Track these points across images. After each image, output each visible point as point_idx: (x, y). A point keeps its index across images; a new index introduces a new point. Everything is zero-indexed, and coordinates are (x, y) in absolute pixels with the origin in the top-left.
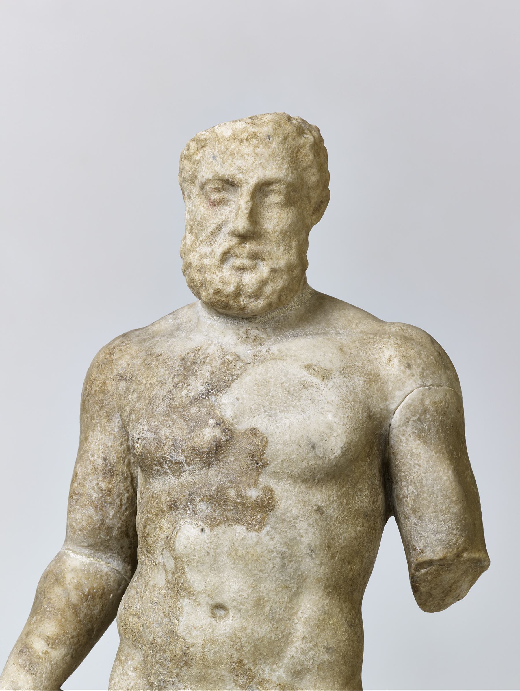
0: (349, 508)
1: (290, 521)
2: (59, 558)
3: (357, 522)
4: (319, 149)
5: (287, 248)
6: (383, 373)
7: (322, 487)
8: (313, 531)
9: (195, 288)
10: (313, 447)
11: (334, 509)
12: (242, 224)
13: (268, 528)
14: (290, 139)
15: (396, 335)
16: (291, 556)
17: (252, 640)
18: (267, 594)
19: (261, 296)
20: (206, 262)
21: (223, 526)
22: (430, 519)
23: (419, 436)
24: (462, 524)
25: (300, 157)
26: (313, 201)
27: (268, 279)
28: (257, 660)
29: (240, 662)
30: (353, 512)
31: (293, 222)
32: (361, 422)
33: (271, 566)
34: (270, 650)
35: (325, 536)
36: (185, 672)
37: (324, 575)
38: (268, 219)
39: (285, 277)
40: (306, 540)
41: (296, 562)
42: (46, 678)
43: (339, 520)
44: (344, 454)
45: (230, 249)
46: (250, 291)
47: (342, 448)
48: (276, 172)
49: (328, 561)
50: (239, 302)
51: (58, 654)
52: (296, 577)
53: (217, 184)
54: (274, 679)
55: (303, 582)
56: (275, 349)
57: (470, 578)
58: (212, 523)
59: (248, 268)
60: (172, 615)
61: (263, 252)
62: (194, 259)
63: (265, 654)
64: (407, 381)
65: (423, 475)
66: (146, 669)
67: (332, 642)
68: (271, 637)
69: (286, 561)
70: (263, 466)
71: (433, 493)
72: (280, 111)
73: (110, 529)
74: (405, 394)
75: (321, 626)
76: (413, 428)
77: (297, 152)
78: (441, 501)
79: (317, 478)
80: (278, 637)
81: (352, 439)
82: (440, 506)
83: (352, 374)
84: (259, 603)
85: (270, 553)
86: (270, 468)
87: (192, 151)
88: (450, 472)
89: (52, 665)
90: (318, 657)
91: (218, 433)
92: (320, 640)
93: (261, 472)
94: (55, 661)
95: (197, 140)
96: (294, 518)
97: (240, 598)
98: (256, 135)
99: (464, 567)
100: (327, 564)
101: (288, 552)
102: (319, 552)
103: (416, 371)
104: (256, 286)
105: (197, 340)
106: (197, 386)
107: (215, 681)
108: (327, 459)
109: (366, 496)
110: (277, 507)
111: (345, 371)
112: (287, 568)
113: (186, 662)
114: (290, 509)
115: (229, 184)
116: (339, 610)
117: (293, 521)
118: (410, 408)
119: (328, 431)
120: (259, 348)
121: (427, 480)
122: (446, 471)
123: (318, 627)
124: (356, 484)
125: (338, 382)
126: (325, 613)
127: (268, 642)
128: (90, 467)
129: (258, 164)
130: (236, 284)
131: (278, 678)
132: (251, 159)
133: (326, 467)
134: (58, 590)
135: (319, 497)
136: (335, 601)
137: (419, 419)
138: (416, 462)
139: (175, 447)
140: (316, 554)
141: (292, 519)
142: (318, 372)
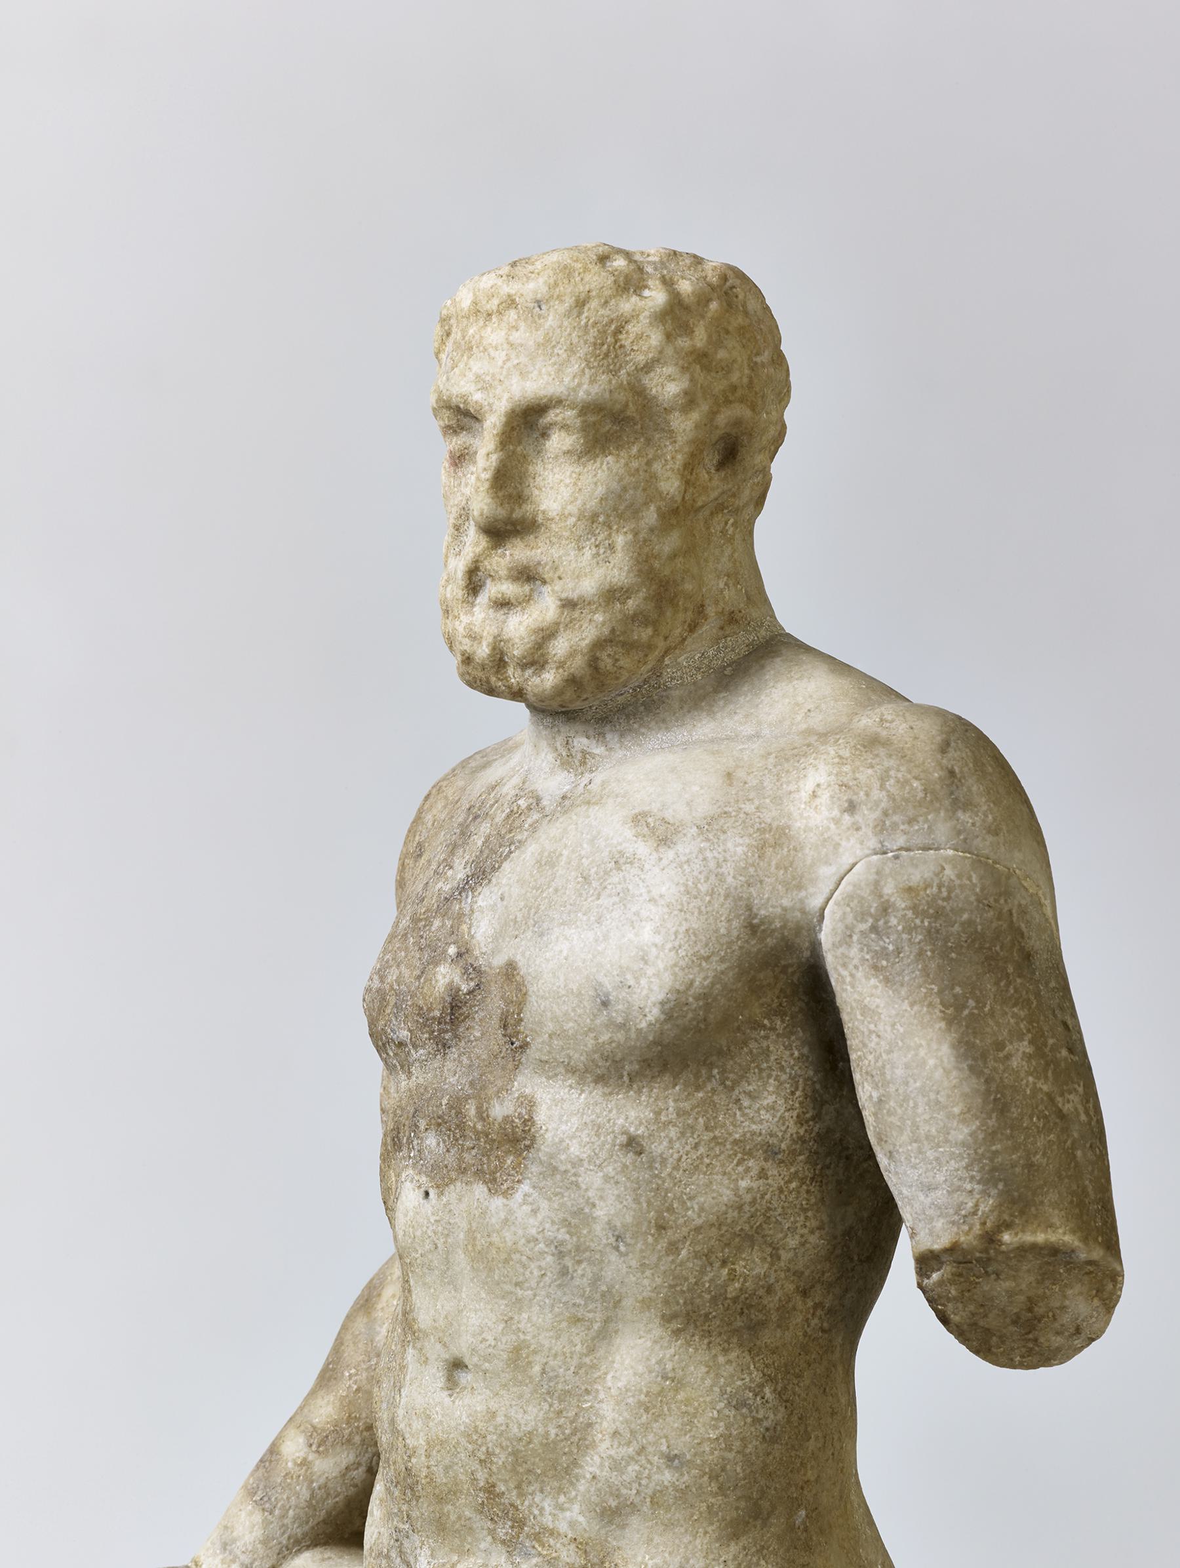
0: (715, 1138)
1: (566, 1172)
3: (740, 1169)
5: (602, 551)
6: (798, 824)
7: (639, 1092)
8: (616, 1192)
10: (605, 1004)
11: (671, 1141)
13: (525, 1187)
14: (594, 304)
17: (508, 1439)
18: (534, 1337)
19: (546, 662)
21: (458, 1184)
22: (908, 1159)
24: (983, 1168)
25: (627, 343)
26: (681, 439)
27: (558, 624)
28: (524, 1486)
29: (490, 1489)
30: (728, 1146)
31: (609, 491)
32: (725, 940)
33: (536, 1273)
35: (649, 1203)
38: (552, 488)
39: (599, 618)
41: (591, 1262)
42: (296, 1518)
43: (684, 1165)
45: (477, 561)
46: (515, 653)
47: (662, 1003)
48: (548, 383)
49: (659, 1259)
50: (506, 678)
52: (597, 1296)
54: (563, 1527)
55: (615, 1307)
59: (513, 601)
61: (539, 563)
63: (539, 1471)
64: (844, 843)
65: (885, 1056)
67: (682, 1444)
68: (547, 1433)
69: (568, 1262)
70: (521, 1047)
75: (655, 1407)
76: (861, 950)
77: (618, 331)
78: (927, 1117)
79: (625, 1073)
80: (564, 1434)
81: (692, 982)
82: (924, 1129)
83: (724, 832)
85: (532, 1244)
86: (533, 1053)
88: (945, 1050)
89: (313, 1491)
90: (649, 1477)
92: (651, 1437)
93: (520, 1063)
94: (322, 1481)
96: (574, 1165)
97: (483, 1346)
98: (513, 301)
100: (657, 1266)
101: (571, 1242)
102: (633, 1242)
103: (868, 816)
107: (457, 1531)
108: (633, 1030)
109: (771, 1108)
110: (539, 1141)
112: (572, 1278)
114: (564, 1144)
116: (704, 1369)
117: (573, 1171)
118: (852, 905)
121: (893, 1067)
122: (934, 1046)
123: (647, 1410)
124: (736, 1083)
125: (687, 851)
126: (665, 1377)
127: (541, 1444)
130: (490, 639)
131: (572, 1524)
133: (635, 1047)
135: (633, 1114)
136: (696, 1350)
137: (874, 929)
138: (872, 1027)
140: (627, 1245)
141: (569, 1167)
142: (653, 830)
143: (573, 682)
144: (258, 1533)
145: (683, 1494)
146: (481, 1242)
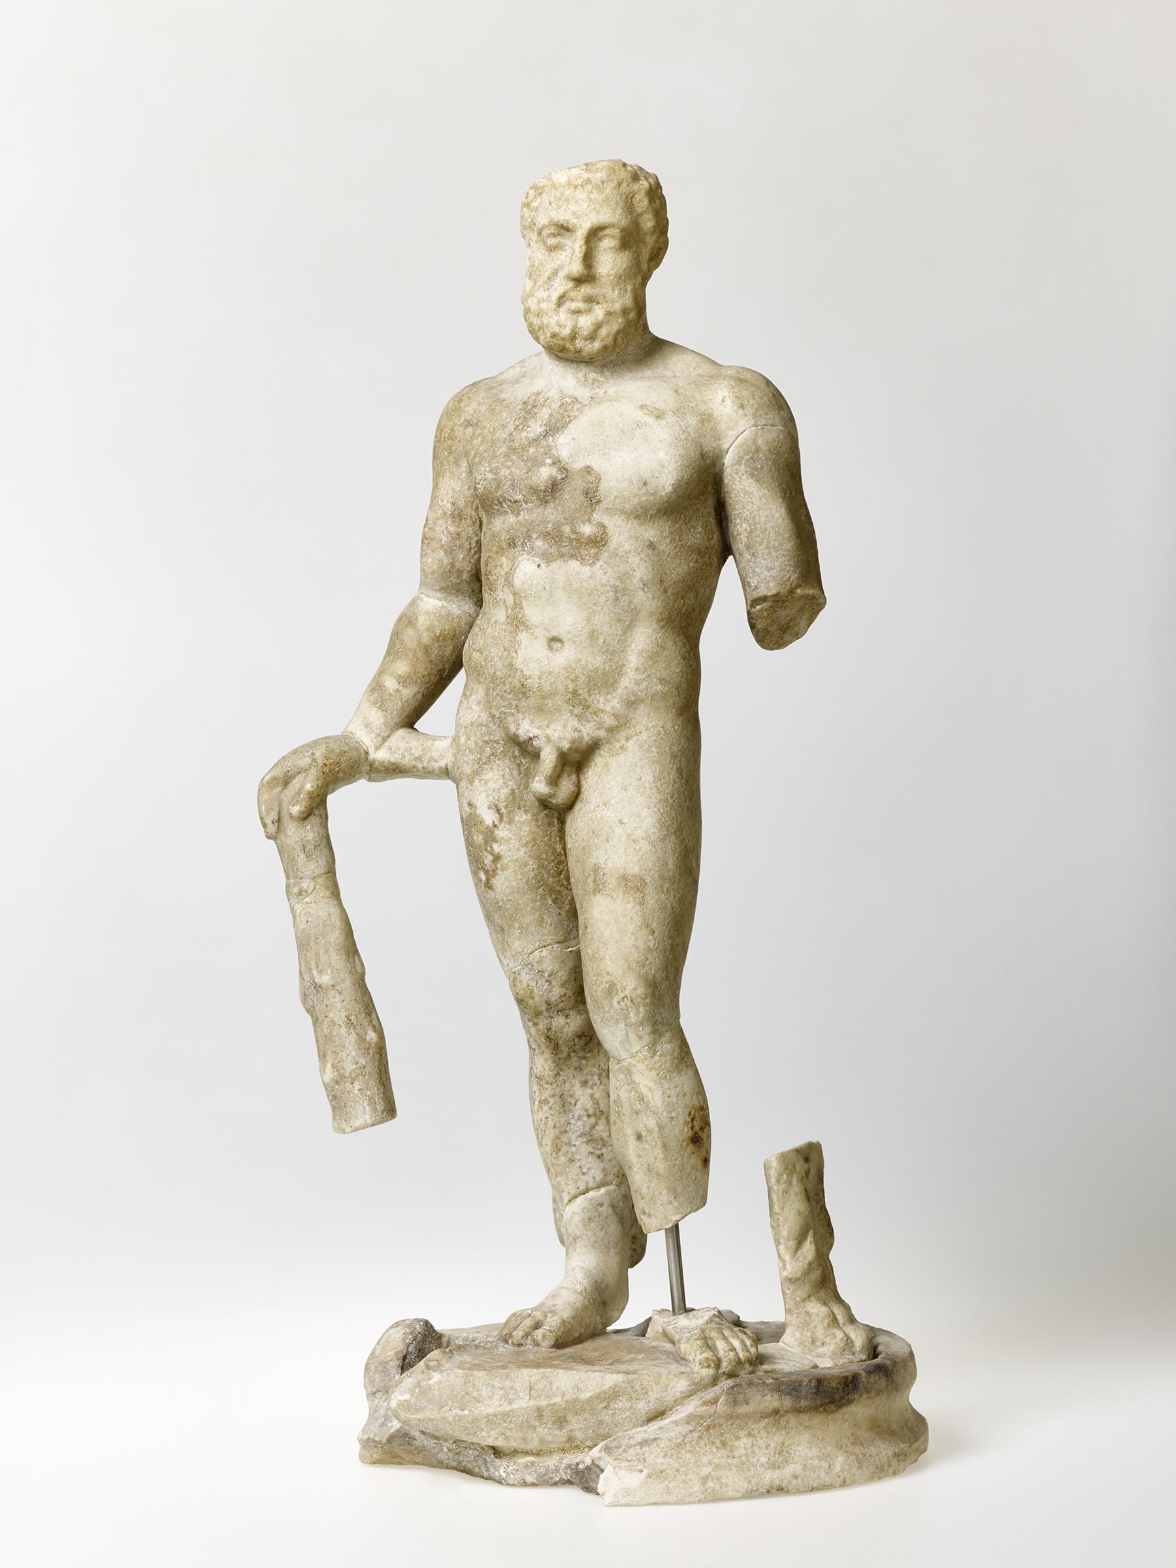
2: (413, 603)
4: (655, 194)
9: (534, 332)
10: (645, 484)
12: (577, 268)
13: (601, 562)
14: (624, 185)
15: (731, 377)
16: (624, 589)
20: (544, 306)
23: (752, 475)
26: (650, 246)
29: (575, 693)
34: (605, 680)
36: (523, 703)
37: (657, 608)
39: (620, 320)
40: (638, 574)
41: (629, 595)
44: (675, 491)
51: (410, 693)
53: (552, 230)
54: (608, 709)
56: (611, 391)
57: (807, 615)
58: (547, 558)
60: (511, 649)
62: (532, 304)
66: (488, 702)
67: (665, 674)
69: (619, 595)
71: (765, 530)
72: (616, 158)
73: (460, 572)
74: (738, 433)
82: (772, 543)
84: (593, 636)
86: (603, 505)
87: (530, 198)
88: (783, 510)
91: (554, 471)
95: (535, 187)
99: (799, 604)
101: (621, 586)
103: (749, 411)
104: (592, 328)
105: (539, 384)
106: (536, 428)
111: (679, 411)
113: (524, 694)
115: (564, 229)
119: (659, 468)
120: (597, 390)
128: (440, 512)
129: (591, 209)
131: (612, 708)
132: (585, 205)
134: (410, 632)
137: (752, 458)
139: (513, 486)
143: (605, 348)
144: (382, 720)
145: (664, 695)
146: (575, 585)
